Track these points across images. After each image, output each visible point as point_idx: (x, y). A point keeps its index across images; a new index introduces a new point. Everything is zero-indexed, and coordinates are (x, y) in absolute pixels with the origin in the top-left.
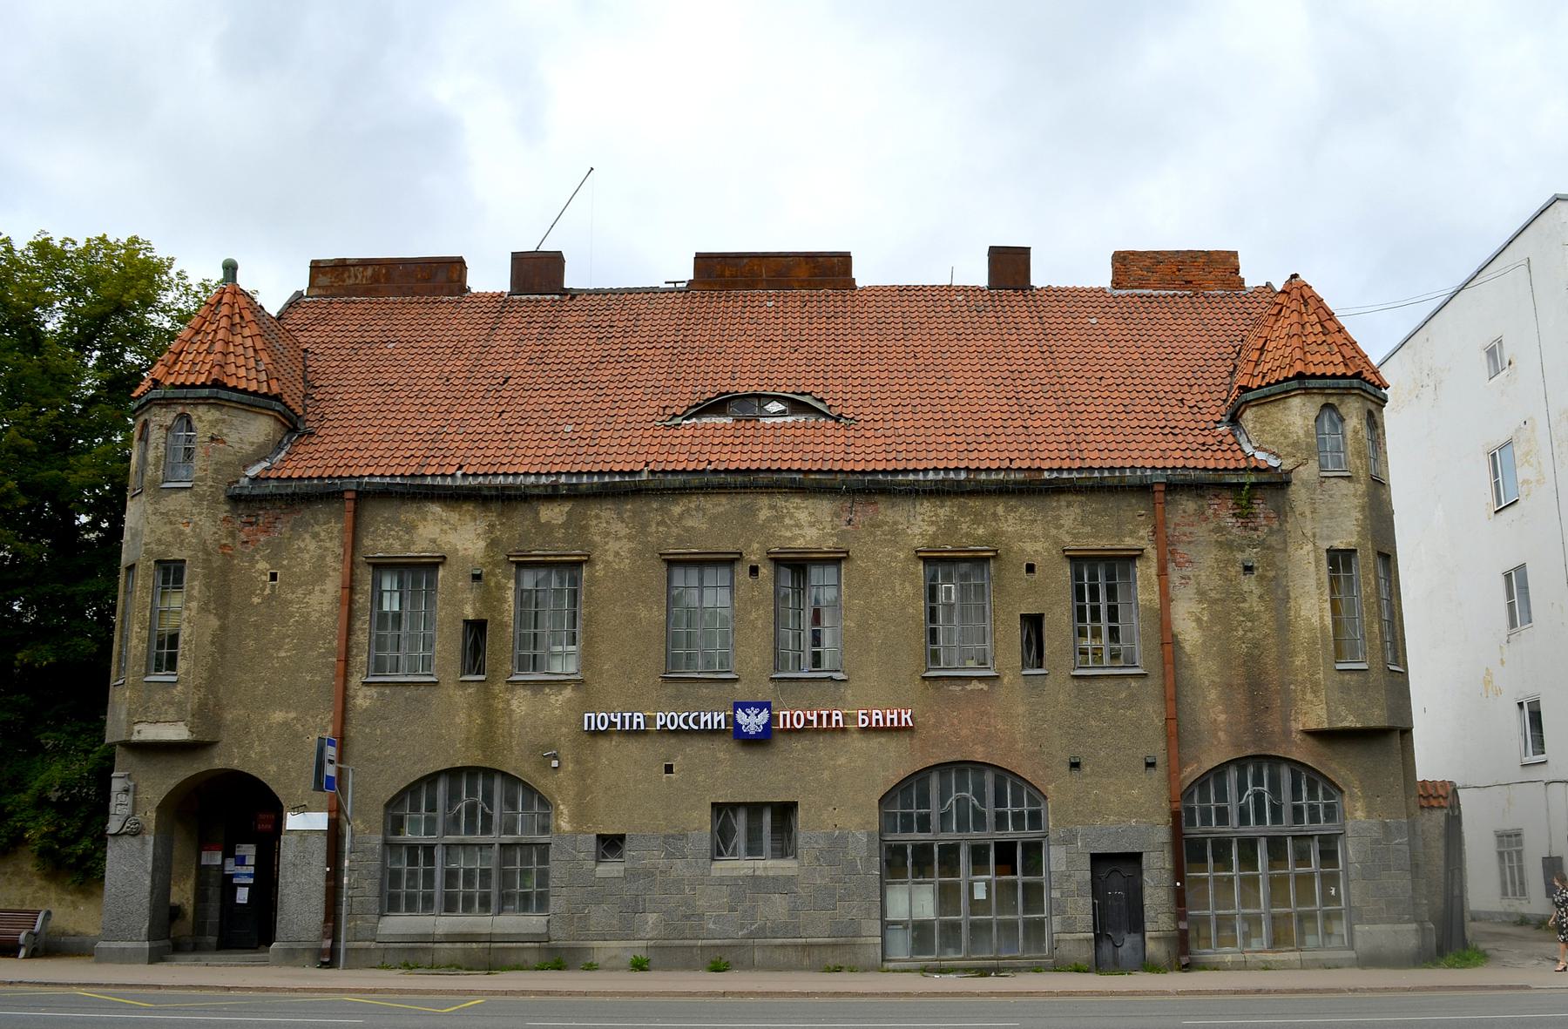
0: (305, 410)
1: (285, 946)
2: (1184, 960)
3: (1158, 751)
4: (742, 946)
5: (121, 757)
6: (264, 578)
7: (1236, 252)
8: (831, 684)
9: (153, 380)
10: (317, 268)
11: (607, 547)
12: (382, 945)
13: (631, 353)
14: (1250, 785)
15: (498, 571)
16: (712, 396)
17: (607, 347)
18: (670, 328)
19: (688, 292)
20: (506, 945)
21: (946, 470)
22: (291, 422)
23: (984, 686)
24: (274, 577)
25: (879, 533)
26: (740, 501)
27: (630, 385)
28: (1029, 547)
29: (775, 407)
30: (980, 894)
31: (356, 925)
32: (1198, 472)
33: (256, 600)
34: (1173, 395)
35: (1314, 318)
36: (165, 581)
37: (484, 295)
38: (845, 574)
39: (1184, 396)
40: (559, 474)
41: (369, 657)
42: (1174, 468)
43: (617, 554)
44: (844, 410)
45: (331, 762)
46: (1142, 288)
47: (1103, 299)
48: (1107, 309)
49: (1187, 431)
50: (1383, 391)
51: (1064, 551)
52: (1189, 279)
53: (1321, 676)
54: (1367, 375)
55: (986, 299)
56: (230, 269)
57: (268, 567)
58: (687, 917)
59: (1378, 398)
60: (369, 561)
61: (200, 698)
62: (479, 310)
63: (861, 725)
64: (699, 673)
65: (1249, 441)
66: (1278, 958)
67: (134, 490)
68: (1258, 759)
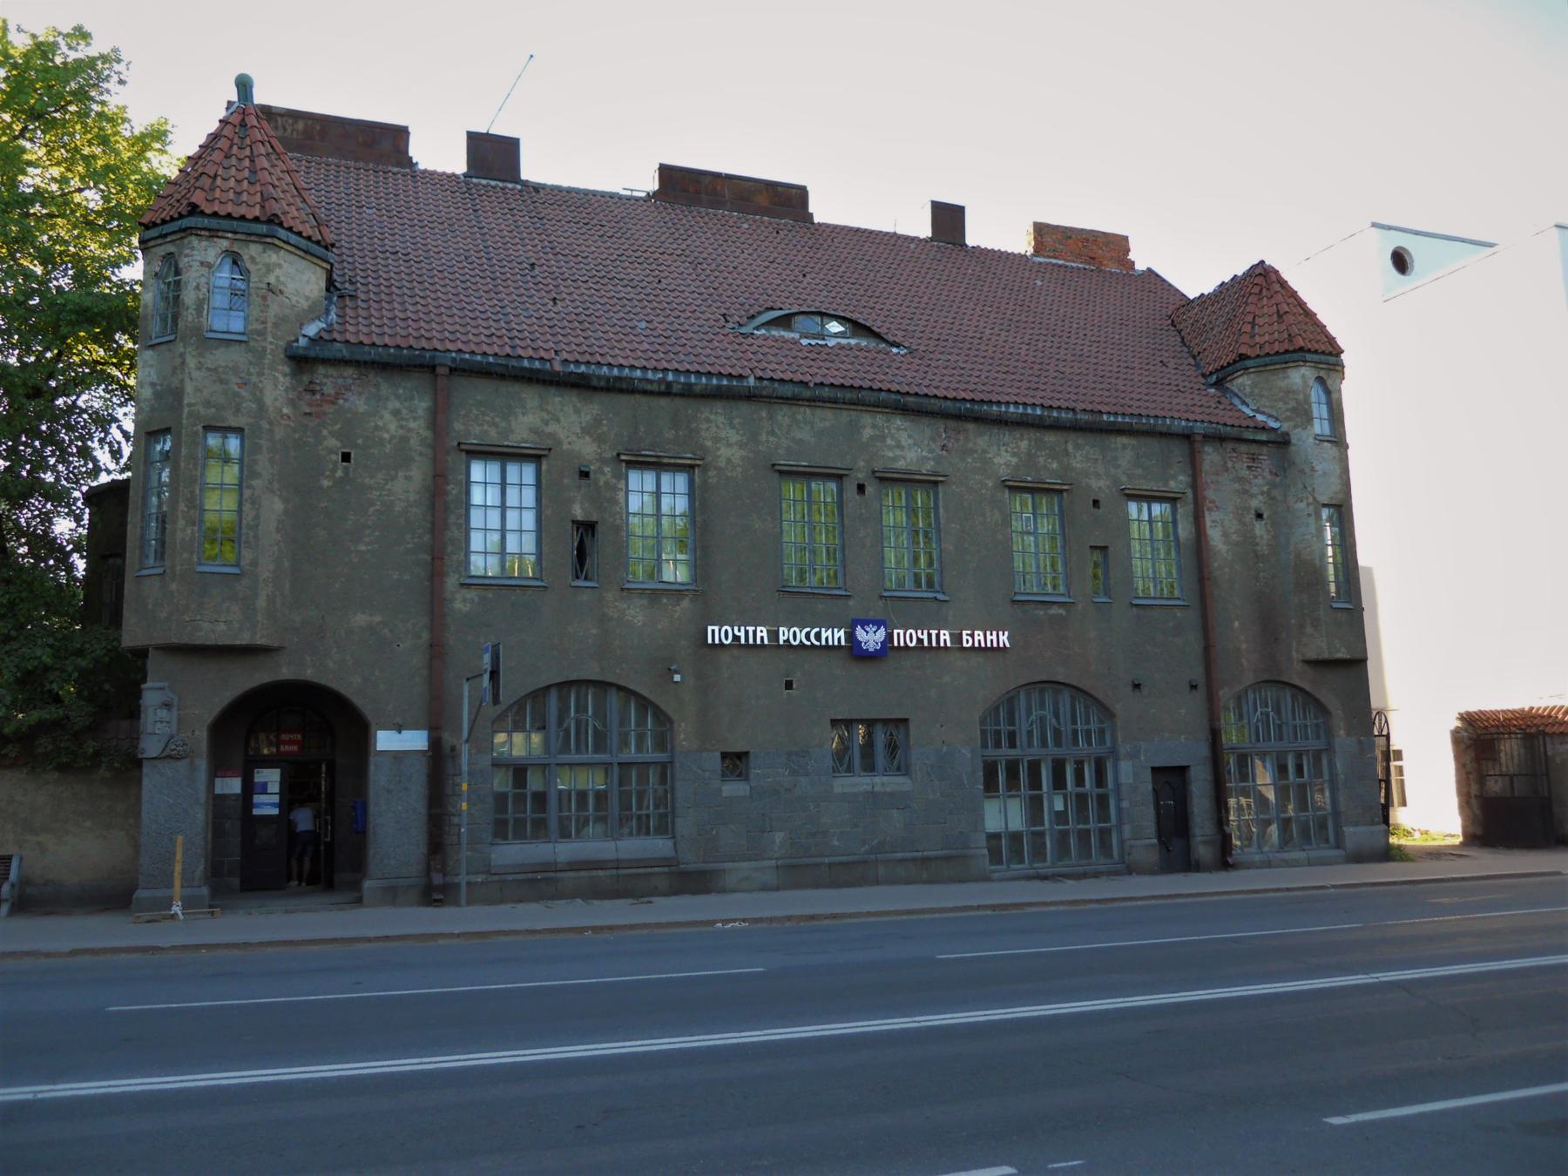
3: (1197, 674)
4: (865, 862)
6: (334, 457)
11: (719, 453)
12: (496, 878)
15: (607, 469)
20: (634, 871)
23: (1062, 611)
24: (346, 457)
26: (845, 416)
28: (1095, 484)
46: (1056, 258)
56: (244, 85)
57: (338, 444)
61: (268, 596)
63: (965, 645)
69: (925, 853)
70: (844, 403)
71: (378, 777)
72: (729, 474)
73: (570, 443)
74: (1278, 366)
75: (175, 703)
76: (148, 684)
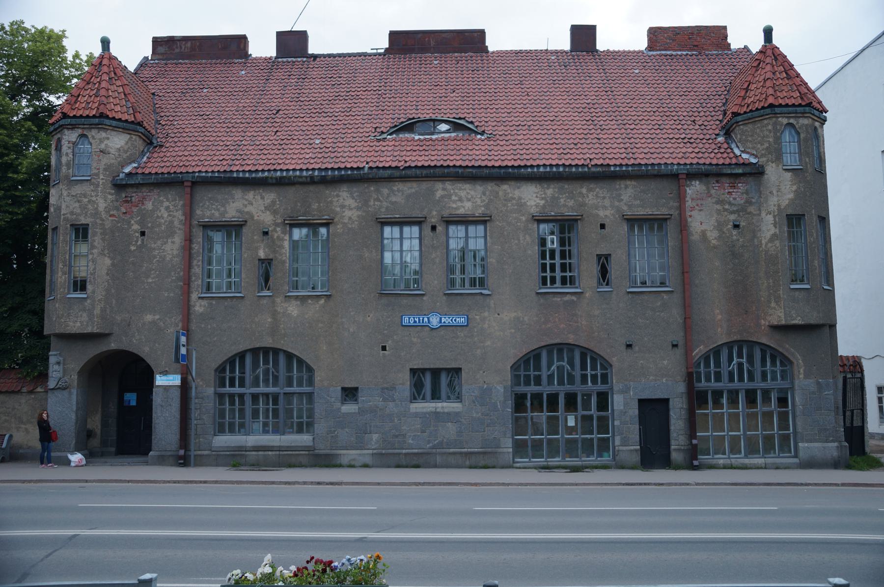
0: (156, 132)
1: (157, 453)
2: (696, 463)
3: (679, 337)
5: (54, 342)
7: (726, 26)
8: (481, 297)
9: (62, 113)
10: (157, 42)
11: (344, 214)
12: (214, 453)
13: (353, 94)
14: (735, 359)
15: (278, 229)
16: (404, 120)
17: (338, 90)
18: (376, 78)
19: (384, 55)
21: (551, 165)
22: (148, 139)
23: (574, 298)
24: (143, 234)
25: (509, 205)
26: (425, 185)
27: (354, 114)
28: (601, 213)
29: (444, 127)
30: (571, 422)
31: (199, 441)
32: (706, 167)
33: (133, 248)
34: (689, 118)
35: (781, 68)
36: (77, 237)
37: (260, 58)
38: (489, 230)
39: (695, 118)
40: (313, 169)
41: (202, 282)
42: (691, 164)
43: (350, 218)
44: (486, 128)
45: (184, 346)
47: (642, 57)
48: (645, 64)
49: (698, 141)
50: (824, 114)
51: (623, 215)
52: (696, 43)
53: (781, 292)
54: (815, 104)
55: (569, 58)
57: (139, 228)
58: (397, 436)
59: (821, 119)
60: (200, 224)
61: (101, 308)
62: (258, 68)
64: (401, 290)
65: (738, 147)
66: (752, 462)
67: (54, 181)
68: (740, 343)
69: (469, 450)
70: (422, 177)
71: (157, 398)
72: (350, 226)
73: (258, 216)
74: (757, 119)
75: (62, 362)
76: (50, 353)
